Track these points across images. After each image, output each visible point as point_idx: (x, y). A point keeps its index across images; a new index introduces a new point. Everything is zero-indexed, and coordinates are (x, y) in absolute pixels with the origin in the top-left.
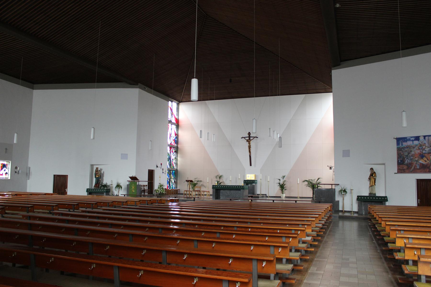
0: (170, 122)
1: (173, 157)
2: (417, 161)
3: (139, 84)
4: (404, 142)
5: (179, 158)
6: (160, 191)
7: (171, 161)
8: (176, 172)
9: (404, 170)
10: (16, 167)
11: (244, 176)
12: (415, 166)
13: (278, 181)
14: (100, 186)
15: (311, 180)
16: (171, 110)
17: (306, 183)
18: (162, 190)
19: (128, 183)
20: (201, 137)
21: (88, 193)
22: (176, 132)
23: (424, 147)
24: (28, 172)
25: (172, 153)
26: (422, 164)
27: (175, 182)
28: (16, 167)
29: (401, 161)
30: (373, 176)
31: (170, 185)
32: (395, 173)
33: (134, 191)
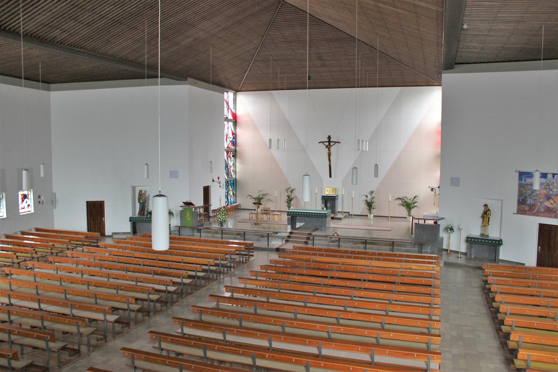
0: (227, 119)
1: (231, 163)
2: (541, 203)
3: (189, 79)
4: (528, 178)
5: (237, 164)
6: (221, 219)
7: (228, 169)
8: (235, 182)
9: (525, 211)
10: (39, 195)
11: (321, 189)
12: (539, 208)
13: (365, 198)
14: (146, 213)
15: (406, 197)
16: (227, 103)
17: (400, 202)
18: (224, 218)
19: (181, 209)
20: (270, 148)
21: (132, 222)
22: (233, 130)
23: (551, 187)
24: (54, 200)
25: (229, 159)
26: (548, 207)
27: (233, 194)
28: (39, 195)
29: (522, 200)
30: (487, 214)
31: (228, 199)
32: (514, 214)
33: (189, 219)
